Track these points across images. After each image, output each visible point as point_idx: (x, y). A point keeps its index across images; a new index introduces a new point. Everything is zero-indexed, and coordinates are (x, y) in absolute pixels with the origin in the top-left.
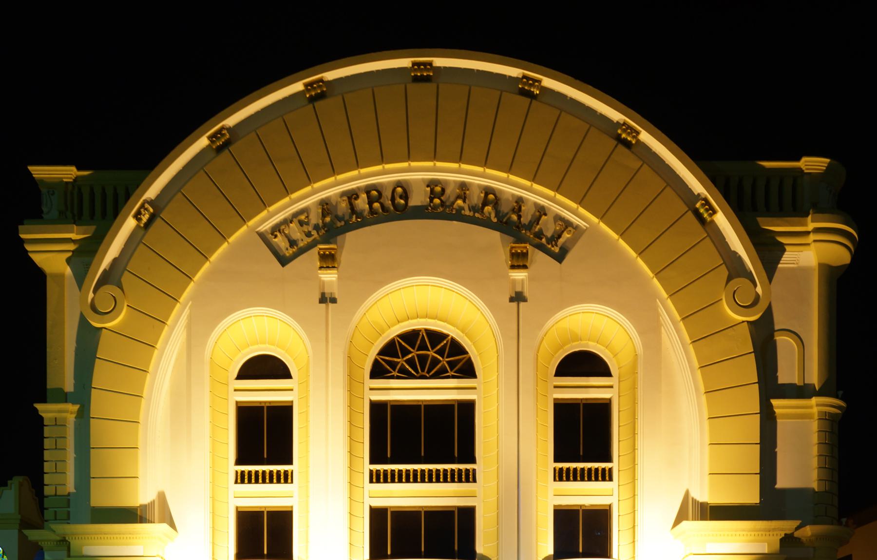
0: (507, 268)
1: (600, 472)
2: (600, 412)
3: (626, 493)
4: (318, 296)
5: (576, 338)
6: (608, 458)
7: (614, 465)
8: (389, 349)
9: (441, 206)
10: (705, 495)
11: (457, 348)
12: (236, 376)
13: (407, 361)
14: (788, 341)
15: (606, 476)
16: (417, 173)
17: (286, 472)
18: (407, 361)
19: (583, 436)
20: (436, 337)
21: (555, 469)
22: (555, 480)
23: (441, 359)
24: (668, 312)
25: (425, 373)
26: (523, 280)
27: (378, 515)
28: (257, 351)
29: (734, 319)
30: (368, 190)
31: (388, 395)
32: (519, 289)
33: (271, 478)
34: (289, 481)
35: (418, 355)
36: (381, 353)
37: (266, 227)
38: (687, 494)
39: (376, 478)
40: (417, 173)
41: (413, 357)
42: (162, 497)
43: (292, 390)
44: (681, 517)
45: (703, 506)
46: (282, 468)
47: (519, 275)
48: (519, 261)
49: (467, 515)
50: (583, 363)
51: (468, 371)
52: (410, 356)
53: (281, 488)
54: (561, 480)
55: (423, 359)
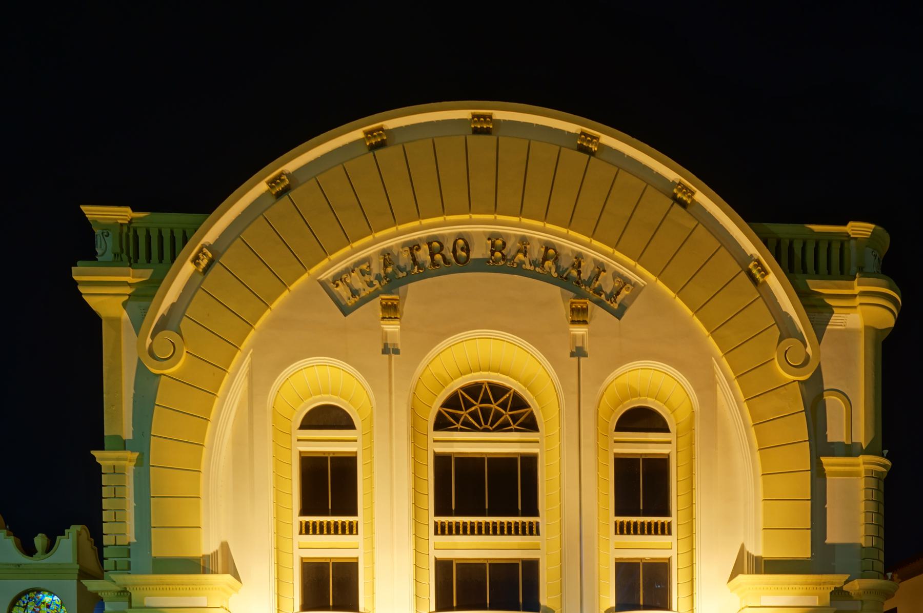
3: (684, 548)
5: (635, 394)
6: (666, 512)
8: (453, 402)
9: (501, 259)
10: (758, 549)
11: (519, 403)
15: (351, 529)
17: (351, 523)
18: (470, 414)
19: (643, 490)
21: (436, 523)
22: (616, 533)
25: (488, 426)
26: (583, 336)
29: (786, 379)
31: (452, 447)
32: (579, 344)
33: (337, 529)
34: (354, 532)
37: (327, 275)
40: (478, 226)
41: (476, 410)
42: (225, 546)
43: (356, 441)
46: (347, 519)
47: (580, 331)
48: (579, 316)
49: (531, 567)
50: (641, 419)
54: (622, 533)
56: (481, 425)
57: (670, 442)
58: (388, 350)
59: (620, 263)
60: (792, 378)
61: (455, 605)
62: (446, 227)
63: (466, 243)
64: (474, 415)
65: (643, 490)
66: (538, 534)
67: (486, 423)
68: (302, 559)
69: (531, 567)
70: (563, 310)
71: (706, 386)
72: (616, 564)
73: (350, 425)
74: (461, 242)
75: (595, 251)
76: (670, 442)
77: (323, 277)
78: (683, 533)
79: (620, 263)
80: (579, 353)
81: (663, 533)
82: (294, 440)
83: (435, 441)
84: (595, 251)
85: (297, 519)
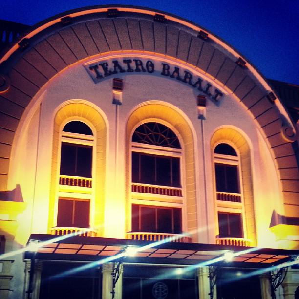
0: (196, 104)
1: (144, 189)
2: (233, 170)
3: (249, 208)
4: (112, 100)
5: (222, 138)
6: (238, 192)
7: (241, 195)
8: (141, 128)
9: (187, 79)
10: (282, 211)
11: (171, 134)
12: (62, 129)
13: (149, 136)
14: (3, 91)
15: (88, 184)
16: (158, 58)
17: (88, 181)
18: (149, 136)
19: (228, 181)
20: (162, 127)
21: (60, 178)
22: (60, 184)
23: (164, 137)
24: (261, 135)
25: (158, 143)
26: (203, 110)
27: (135, 208)
28: (75, 119)
29: (284, 140)
30: (136, 61)
31: (83, 142)
32: (202, 114)
33: (60, 182)
34: (89, 186)
35: (155, 134)
36: (137, 130)
37: (88, 64)
38: (274, 212)
39: (63, 182)
40: (158, 58)
41: (152, 134)
42: (18, 187)
43: (93, 141)
44: (273, 224)
45: (283, 217)
46: (86, 179)
47: (201, 108)
48: (202, 102)
49: (178, 211)
50: (224, 149)
51: (176, 144)
52: (163, 136)
53: (85, 189)
54: (135, 191)
55: (157, 136)
56: (153, 140)
57: (237, 161)
58: (116, 102)
59: (217, 85)
60: (288, 140)
61: (73, 223)
62: (145, 56)
63: (152, 63)
64: (151, 136)
65: (228, 181)
66: (91, 187)
67: (157, 141)
68: (59, 197)
69: (178, 211)
70: (194, 101)
71: (255, 140)
72: (59, 200)
73: (90, 133)
74: (150, 63)
75: (207, 78)
76: (237, 161)
77: (85, 64)
78: (248, 202)
79: (217, 85)
80: (201, 117)
81: (88, 186)
82: (131, 146)
83: (133, 146)
84: (207, 78)
85: (58, 176)
